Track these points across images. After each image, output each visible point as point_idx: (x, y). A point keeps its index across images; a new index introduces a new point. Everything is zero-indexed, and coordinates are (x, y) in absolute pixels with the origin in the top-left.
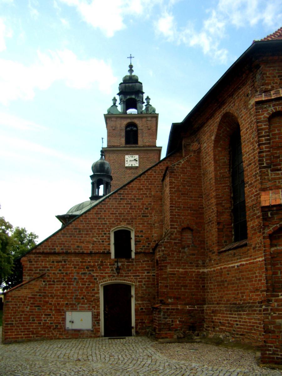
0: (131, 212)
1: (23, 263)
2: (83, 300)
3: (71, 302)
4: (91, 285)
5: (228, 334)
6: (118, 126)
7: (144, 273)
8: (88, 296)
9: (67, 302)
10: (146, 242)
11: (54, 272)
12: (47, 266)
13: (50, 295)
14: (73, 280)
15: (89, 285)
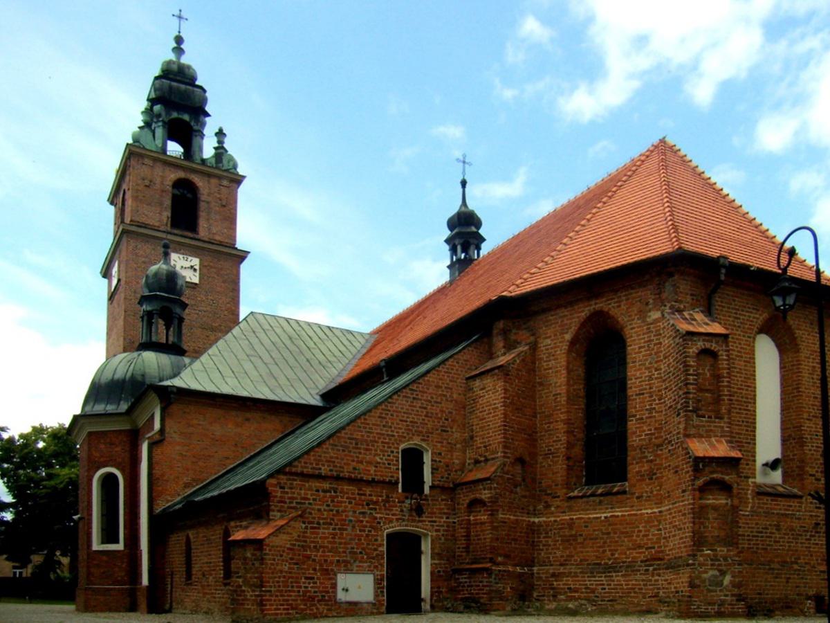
0: (426, 422)
1: (270, 488)
2: (361, 555)
3: (345, 558)
4: (373, 533)
6: (158, 180)
7: (442, 518)
8: (368, 549)
9: (337, 558)
10: (446, 471)
11: (319, 507)
12: (309, 496)
13: (312, 545)
14: (347, 522)
15: (370, 531)
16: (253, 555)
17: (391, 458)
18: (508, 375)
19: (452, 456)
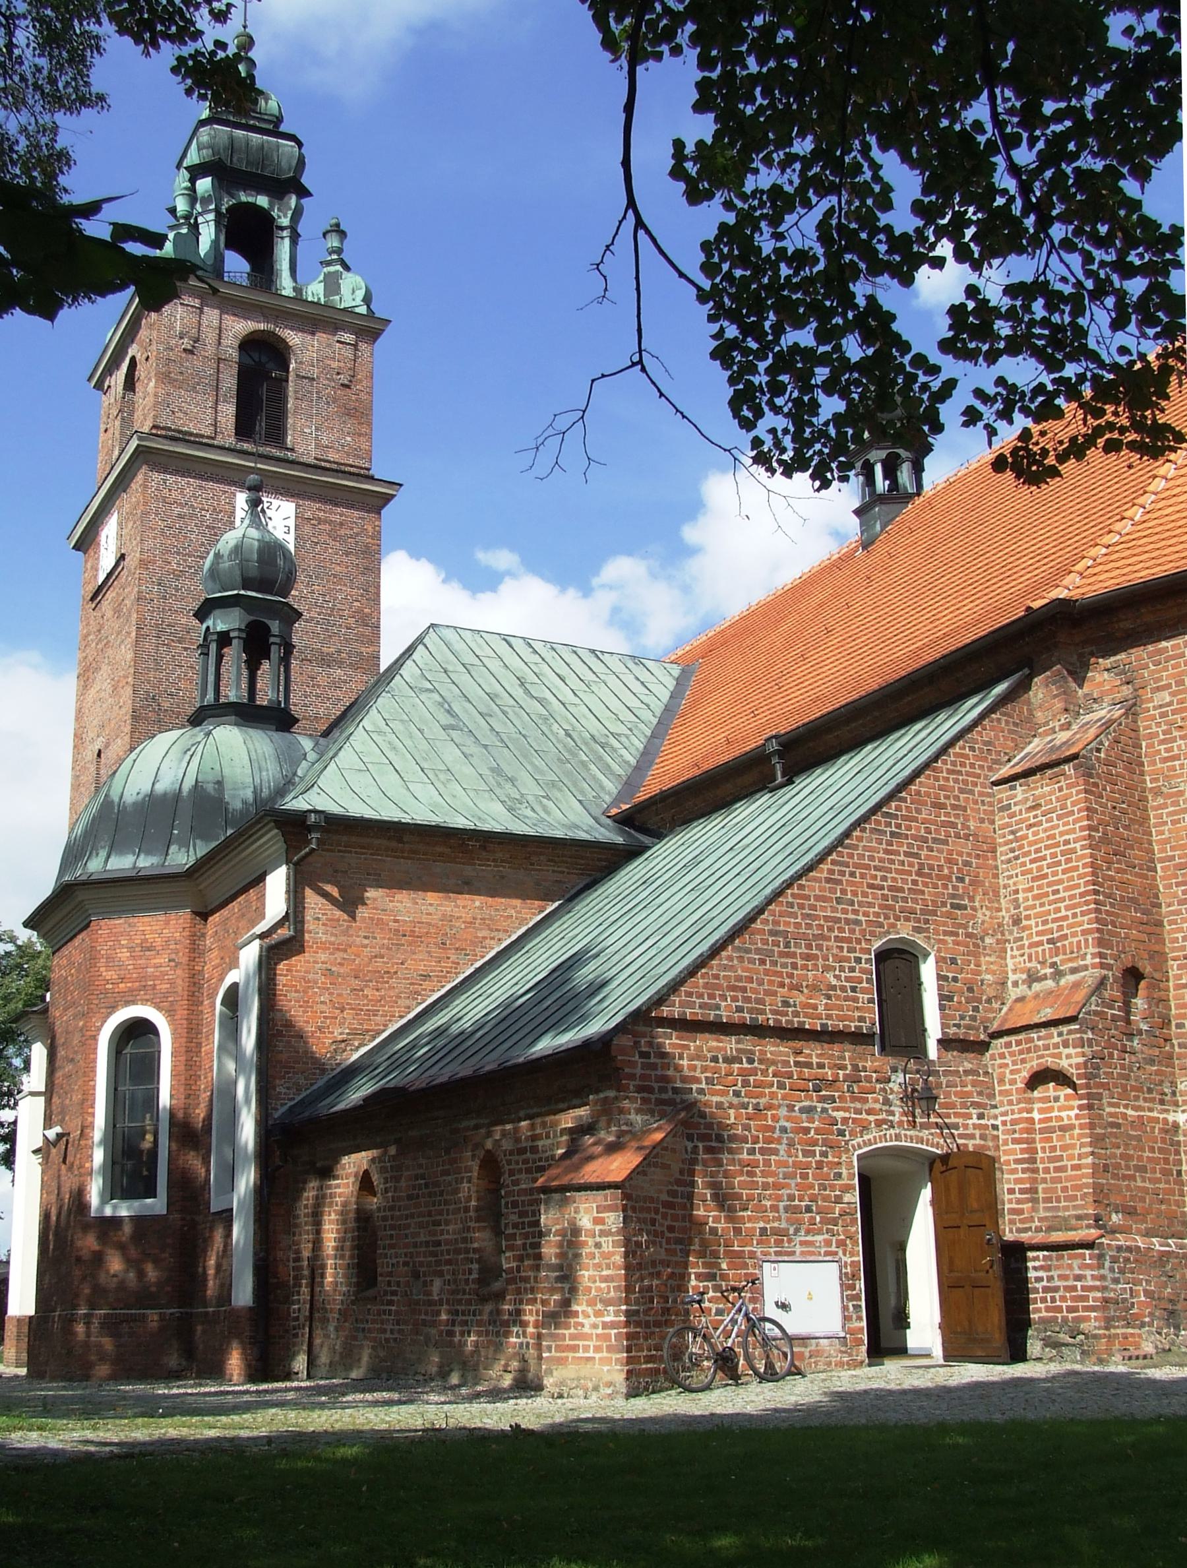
3: (776, 1225)
6: (210, 337)
8: (824, 1200)
9: (762, 1224)
16: (597, 1221)
17: (857, 974)
18: (1090, 776)
19: (978, 965)
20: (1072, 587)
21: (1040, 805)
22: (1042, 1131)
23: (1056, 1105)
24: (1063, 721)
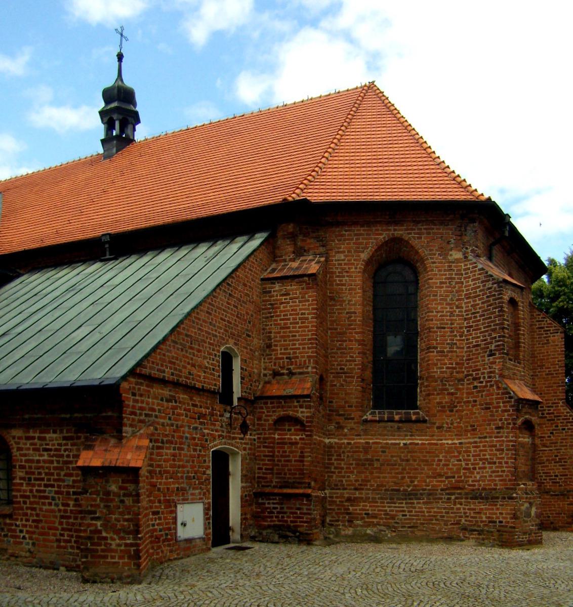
1: (123, 395)
3: (182, 485)
5: (382, 528)
9: (177, 486)
20: (316, 196)
21: (289, 294)
22: (278, 443)
23: (289, 433)
24: (291, 257)
